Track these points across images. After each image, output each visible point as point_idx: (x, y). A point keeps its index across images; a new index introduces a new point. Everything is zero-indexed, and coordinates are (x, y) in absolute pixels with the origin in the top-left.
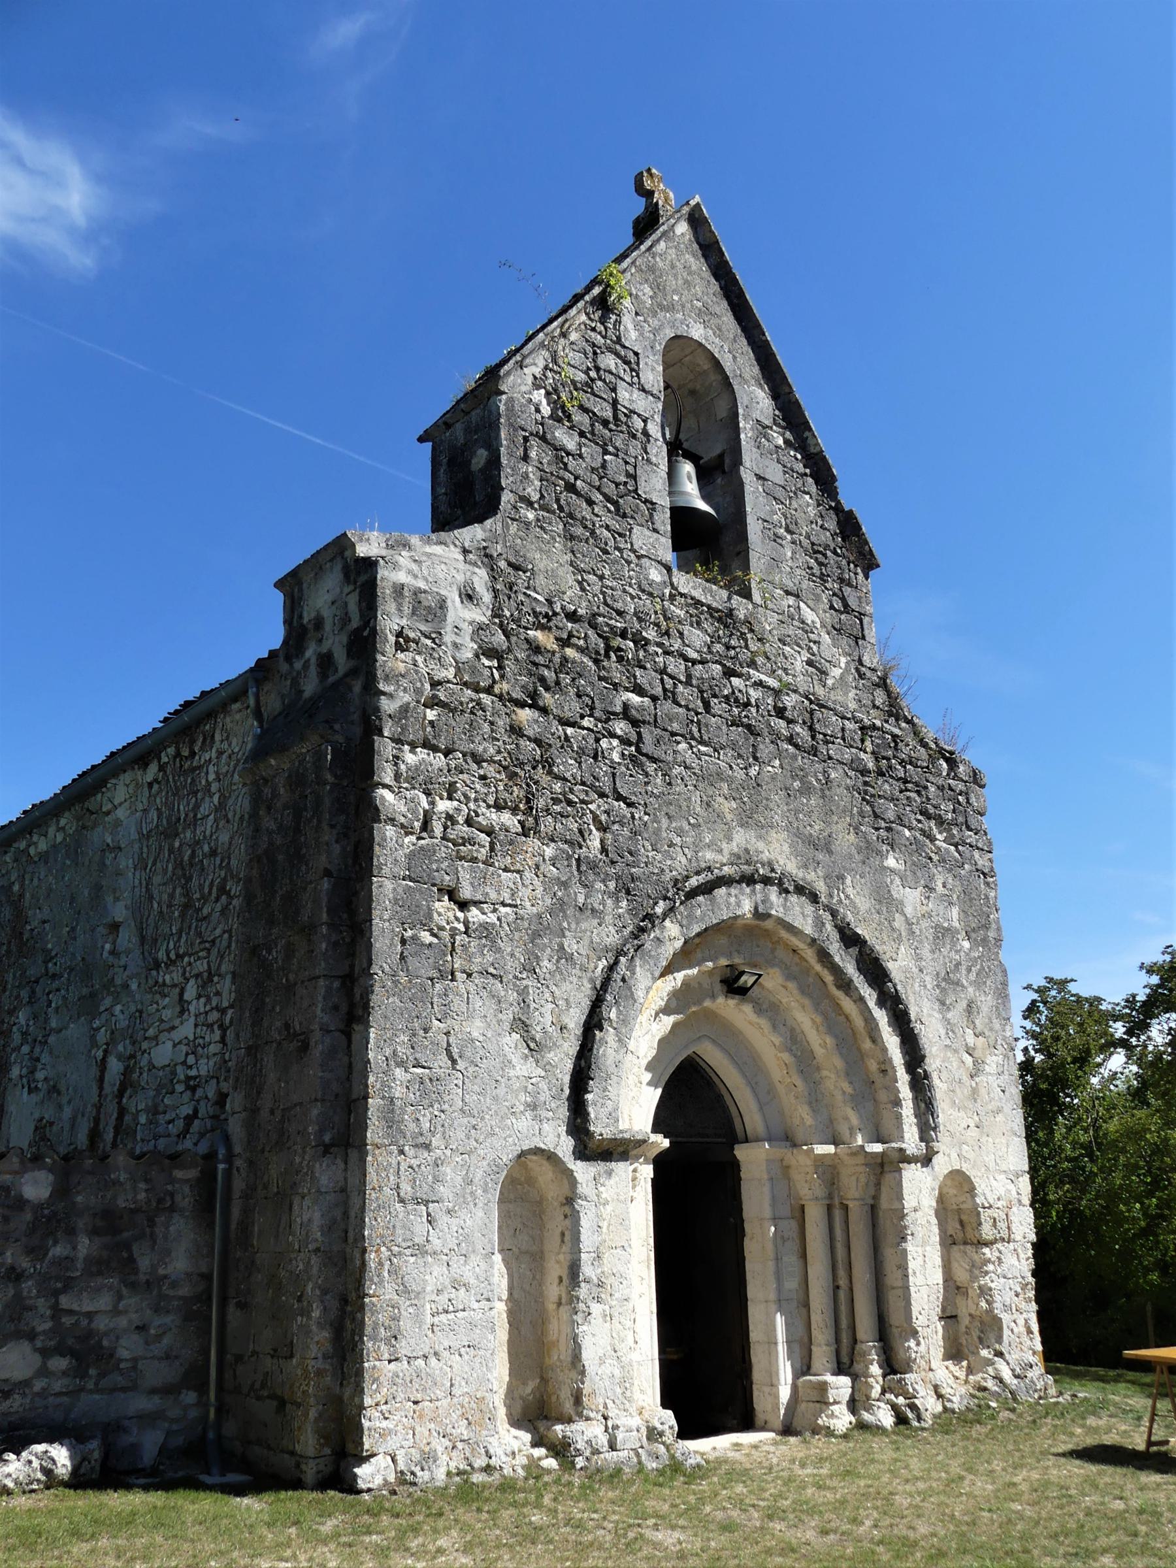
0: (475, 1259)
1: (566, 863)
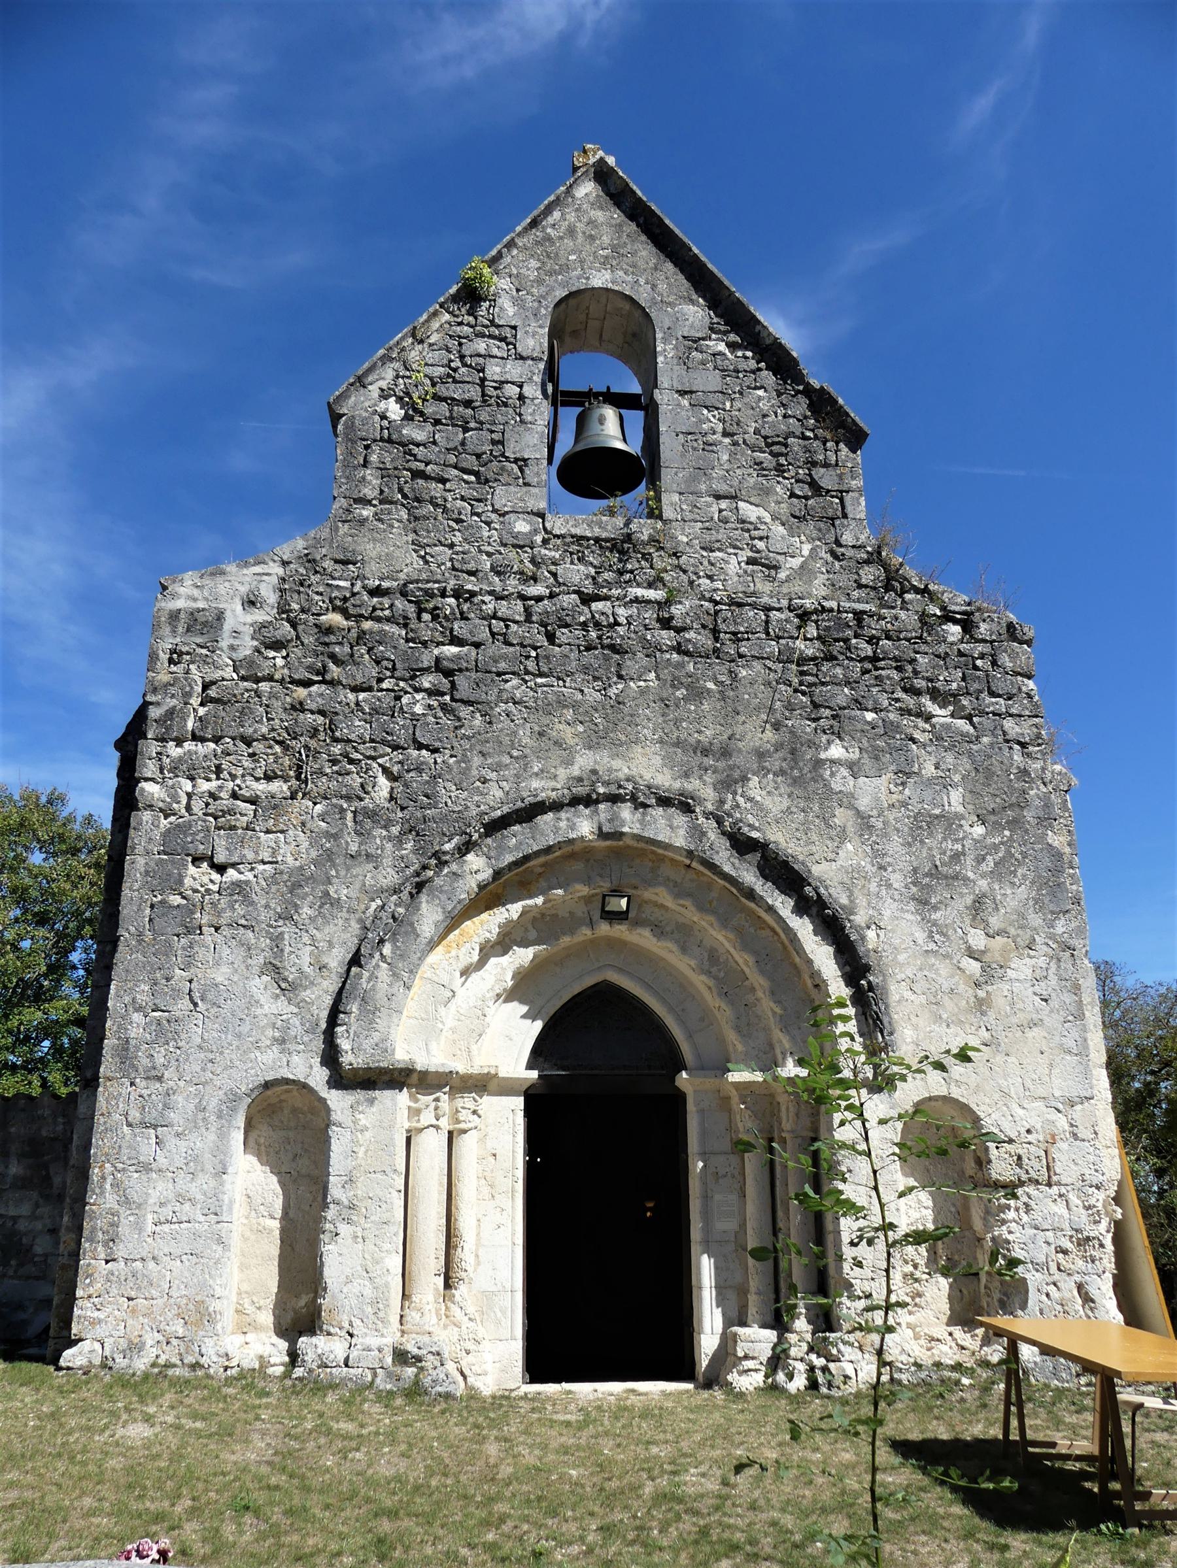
0: (202, 1179)
1: (338, 817)
